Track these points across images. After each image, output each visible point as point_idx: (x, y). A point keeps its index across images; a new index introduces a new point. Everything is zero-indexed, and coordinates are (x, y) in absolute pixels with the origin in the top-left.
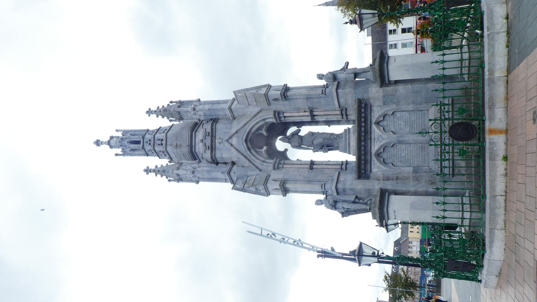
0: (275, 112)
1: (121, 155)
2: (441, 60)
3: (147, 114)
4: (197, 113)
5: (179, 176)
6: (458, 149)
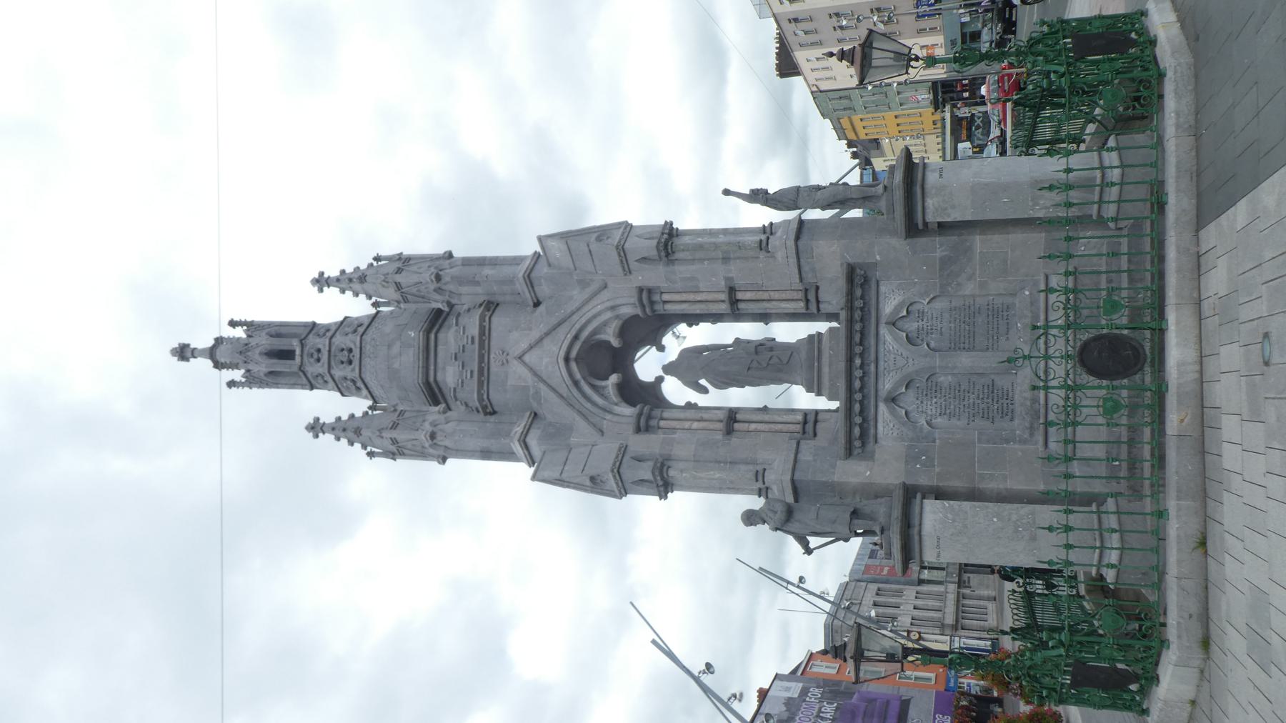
0: (641, 290)
2: (1061, 184)
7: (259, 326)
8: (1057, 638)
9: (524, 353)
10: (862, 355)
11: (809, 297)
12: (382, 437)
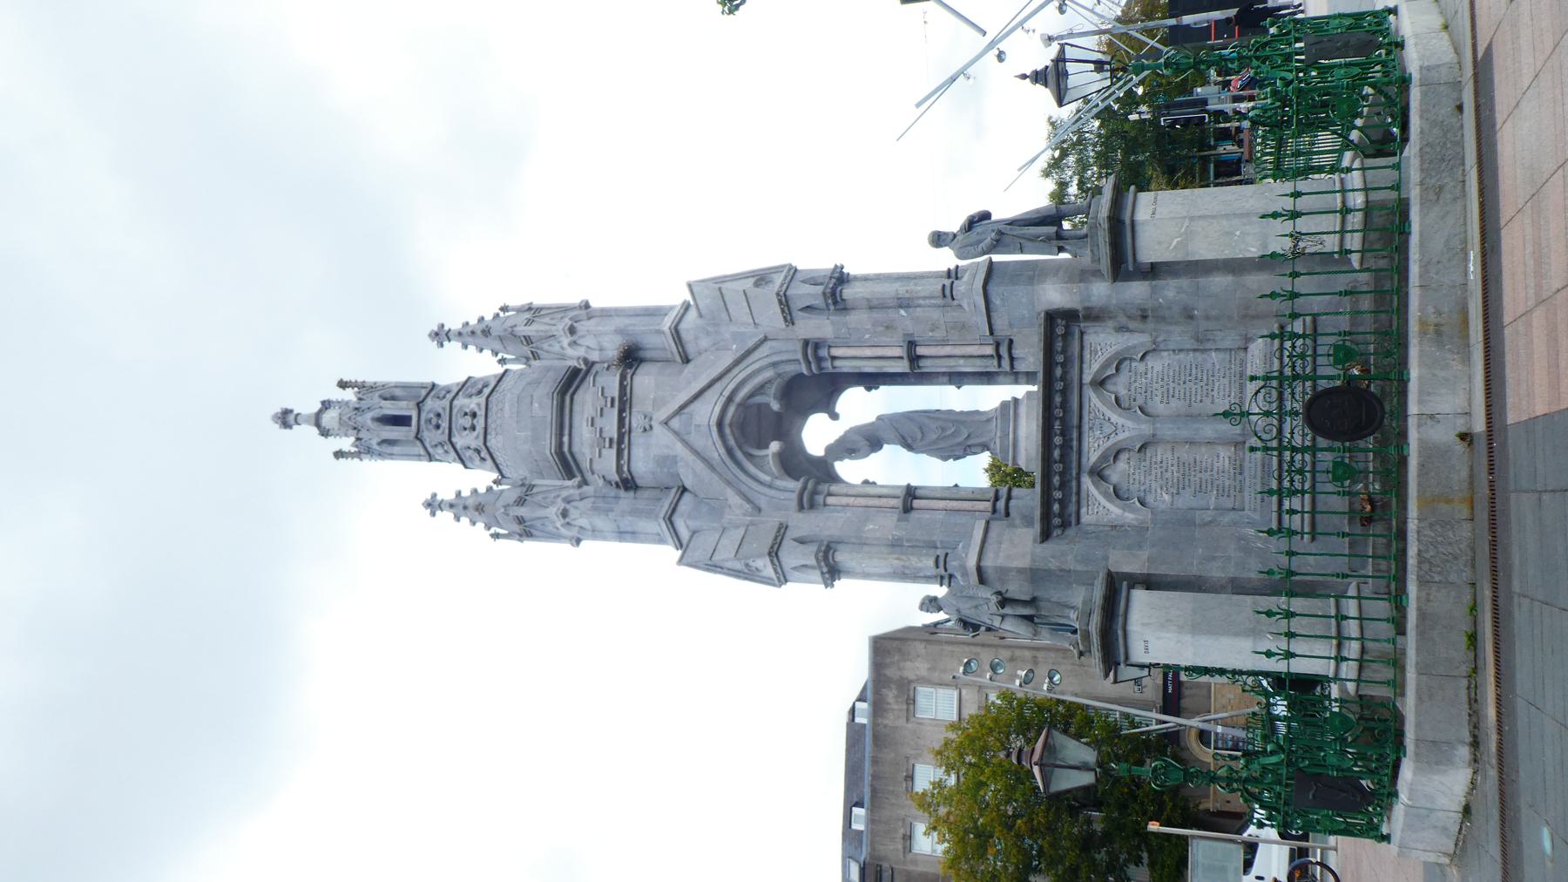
3: (426, 509)
10: (1064, 365)
11: (1001, 353)
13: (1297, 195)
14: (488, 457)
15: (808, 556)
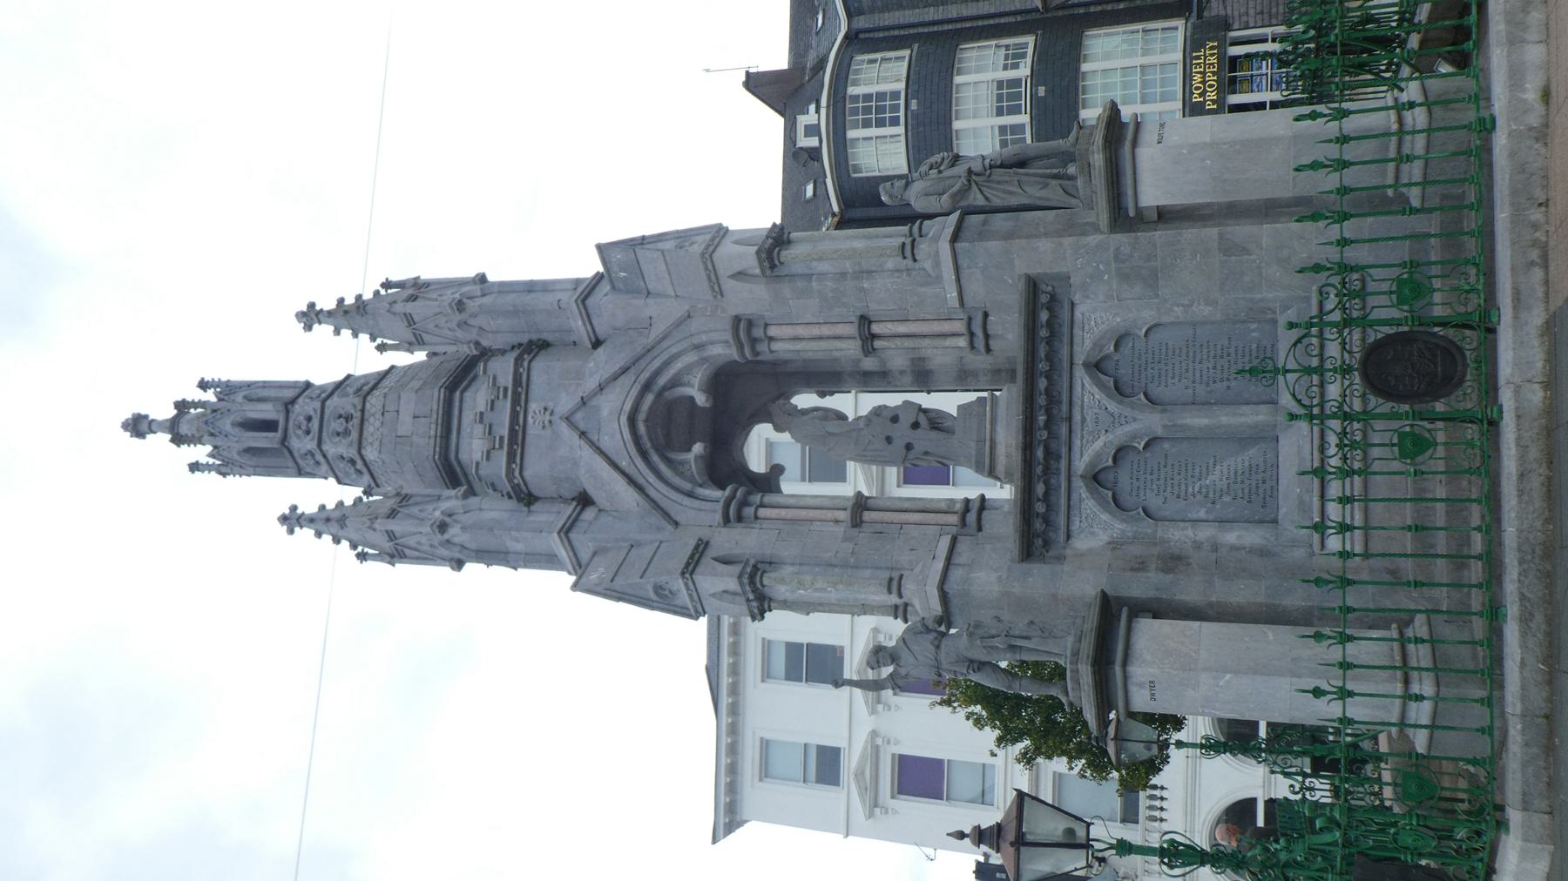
1: (208, 468)
2: (1330, 160)
3: (282, 524)
4: (472, 322)
5: (396, 539)
6: (1395, 431)
7: (236, 387)
8: (1328, 814)
9: (573, 413)
11: (974, 330)
12: (374, 530)
13: (1345, 666)
14: (364, 470)
15: (726, 580)
